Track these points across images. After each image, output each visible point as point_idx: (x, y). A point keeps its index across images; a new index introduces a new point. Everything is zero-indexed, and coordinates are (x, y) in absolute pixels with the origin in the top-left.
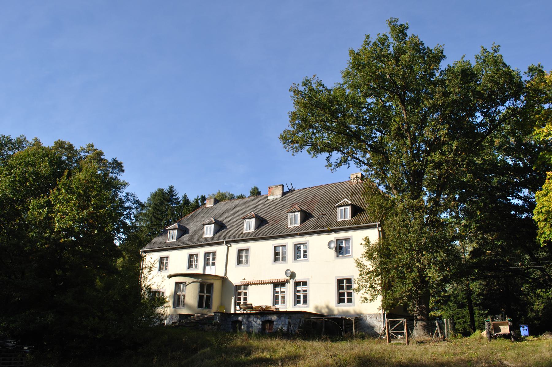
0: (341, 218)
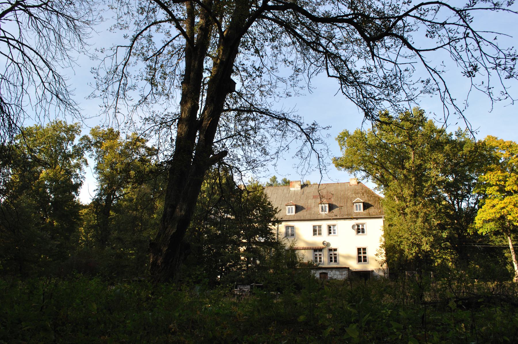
0: (357, 210)
